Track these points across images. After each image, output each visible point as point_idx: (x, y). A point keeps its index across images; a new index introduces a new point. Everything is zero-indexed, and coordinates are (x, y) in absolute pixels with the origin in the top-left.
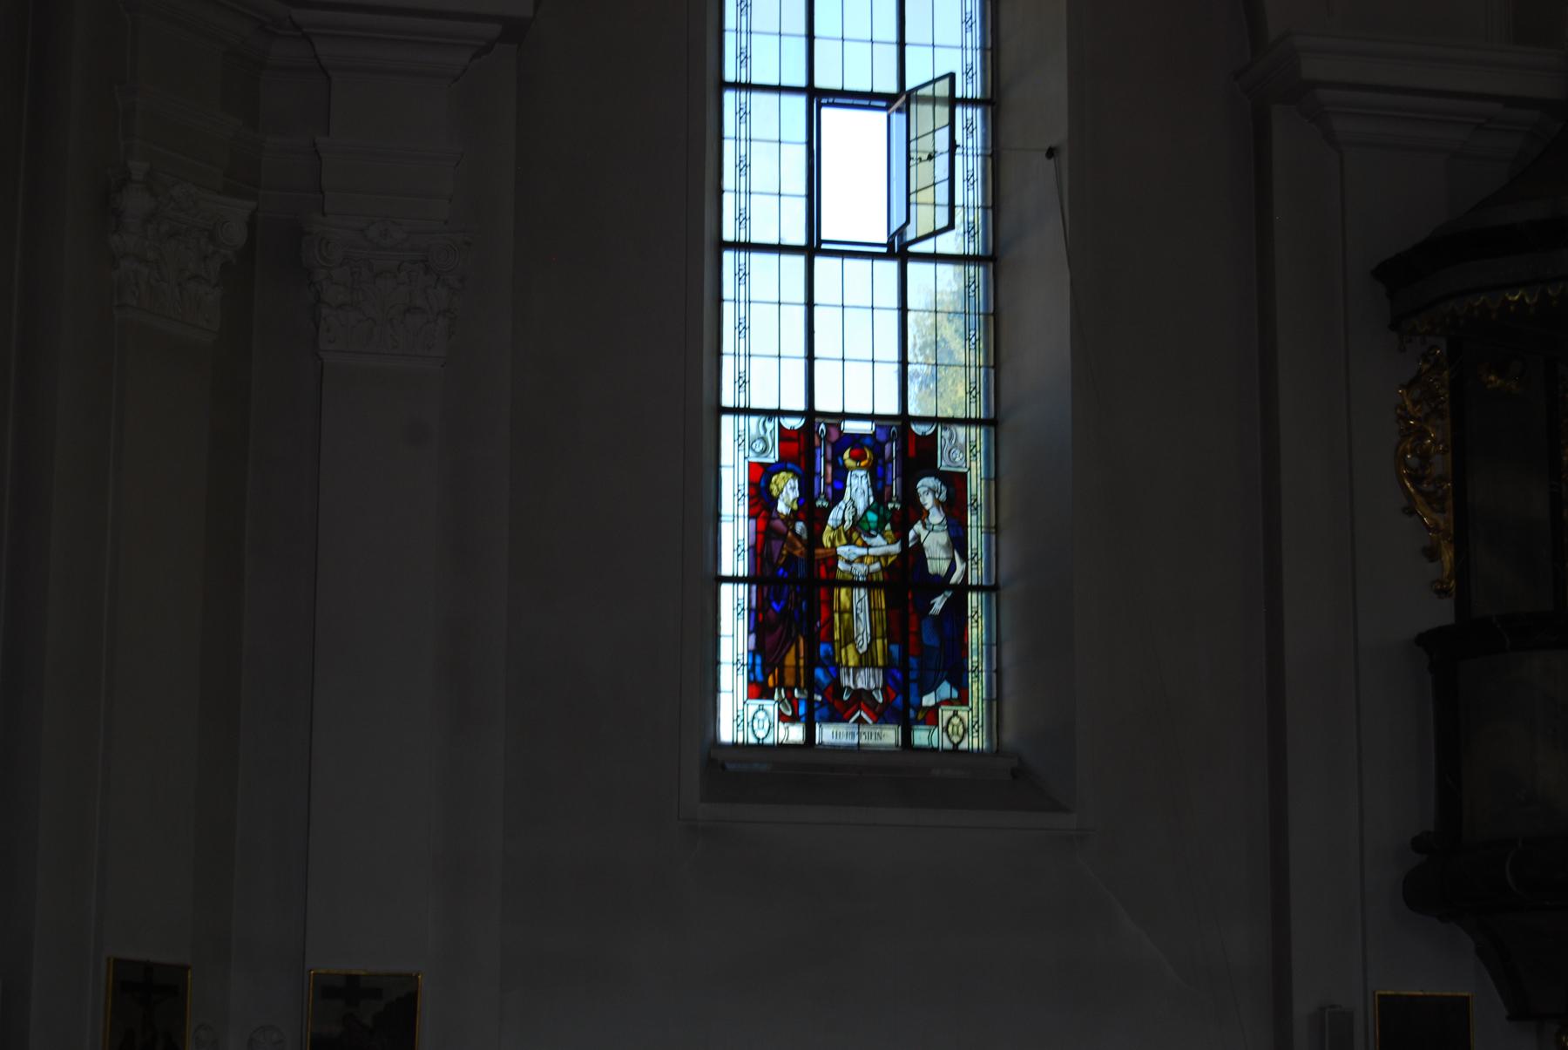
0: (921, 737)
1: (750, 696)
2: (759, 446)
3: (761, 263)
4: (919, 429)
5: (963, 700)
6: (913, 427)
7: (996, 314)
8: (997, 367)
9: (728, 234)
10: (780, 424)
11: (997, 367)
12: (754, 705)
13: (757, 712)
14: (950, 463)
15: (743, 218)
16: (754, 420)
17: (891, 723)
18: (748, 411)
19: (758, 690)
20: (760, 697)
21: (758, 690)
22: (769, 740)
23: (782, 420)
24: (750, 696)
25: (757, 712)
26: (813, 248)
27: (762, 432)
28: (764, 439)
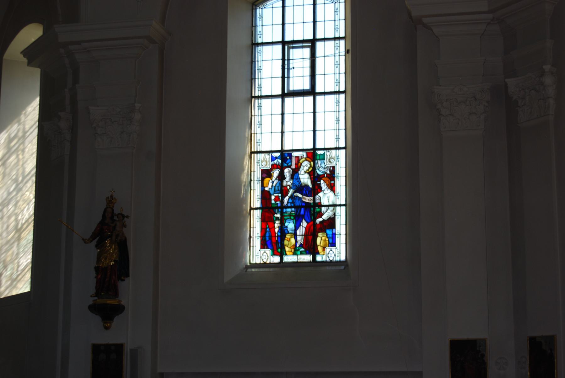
0: (319, 258)
1: (261, 248)
2: (264, 164)
3: (331, 88)
4: (319, 152)
5: (333, 244)
6: (317, 152)
7: (252, 79)
8: (252, 61)
9: (342, 96)
10: (271, 155)
11: (252, 61)
12: (263, 250)
13: (263, 253)
14: (329, 163)
15: (337, 102)
16: (263, 155)
17: (309, 254)
18: (261, 152)
19: (264, 245)
20: (264, 248)
21: (264, 245)
22: (268, 262)
23: (272, 154)
24: (261, 248)
25: (263, 253)
26: (284, 95)
27: (265, 159)
28: (266, 161)
